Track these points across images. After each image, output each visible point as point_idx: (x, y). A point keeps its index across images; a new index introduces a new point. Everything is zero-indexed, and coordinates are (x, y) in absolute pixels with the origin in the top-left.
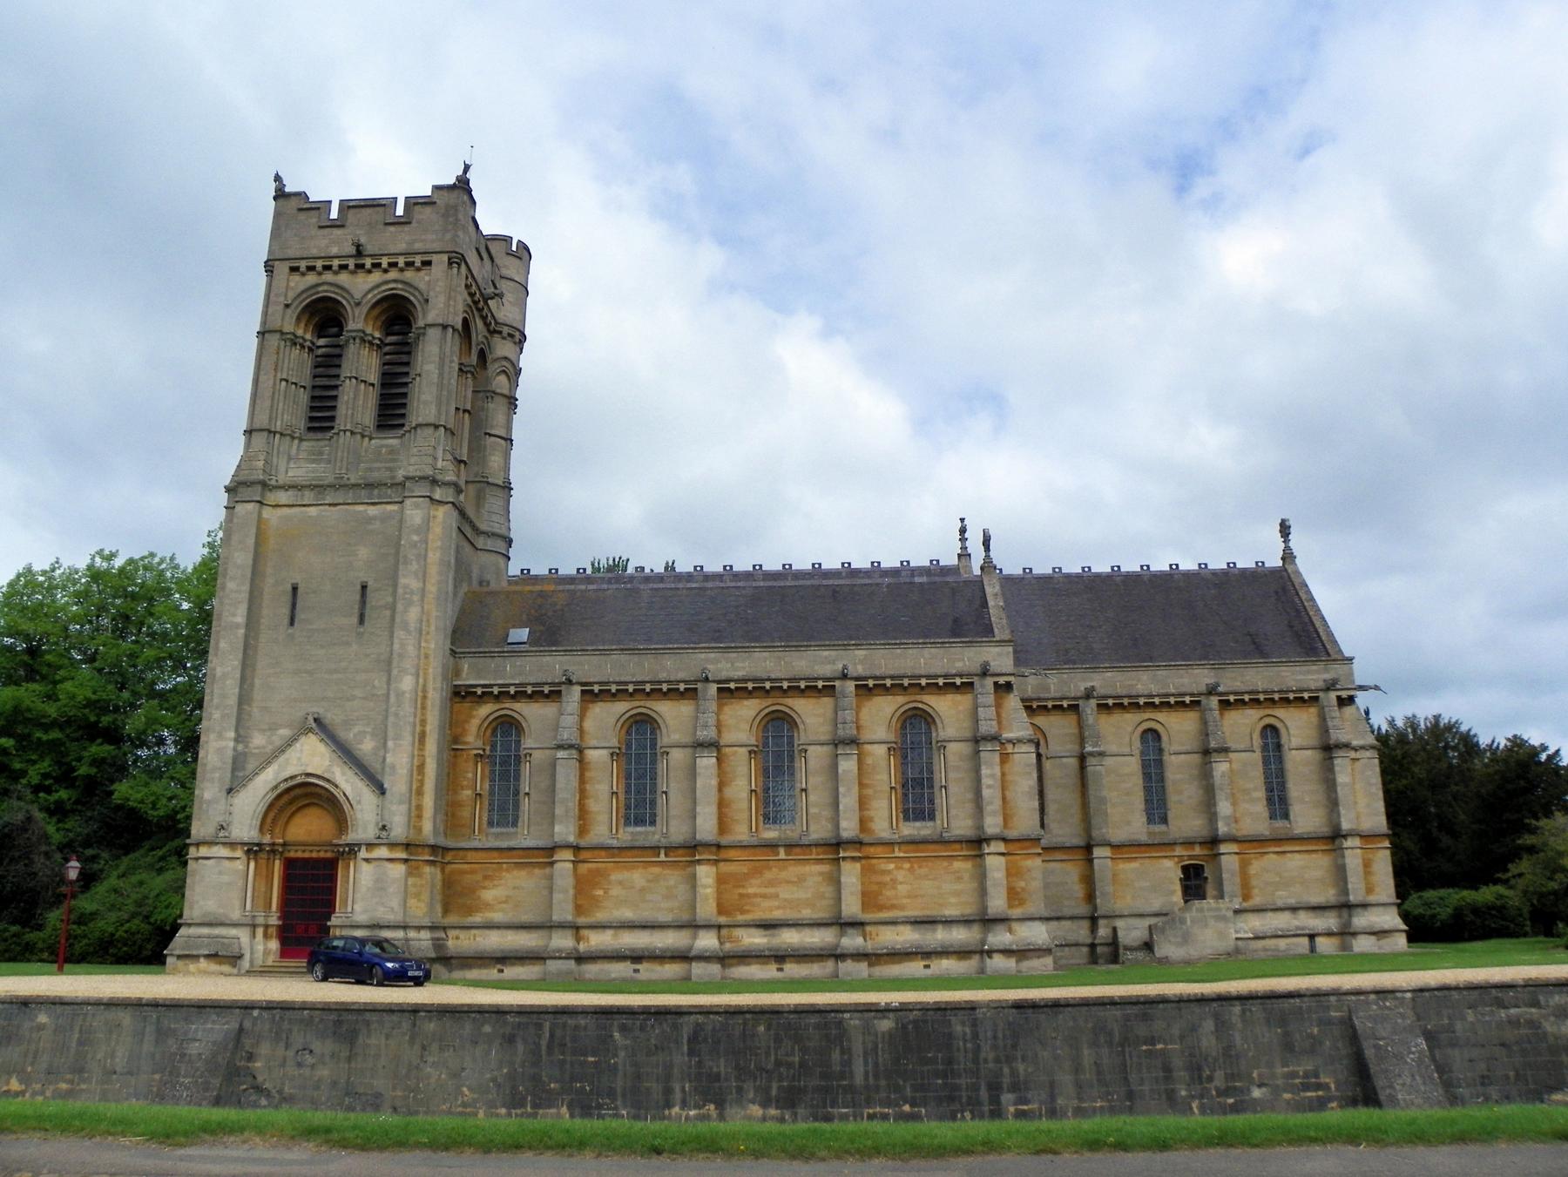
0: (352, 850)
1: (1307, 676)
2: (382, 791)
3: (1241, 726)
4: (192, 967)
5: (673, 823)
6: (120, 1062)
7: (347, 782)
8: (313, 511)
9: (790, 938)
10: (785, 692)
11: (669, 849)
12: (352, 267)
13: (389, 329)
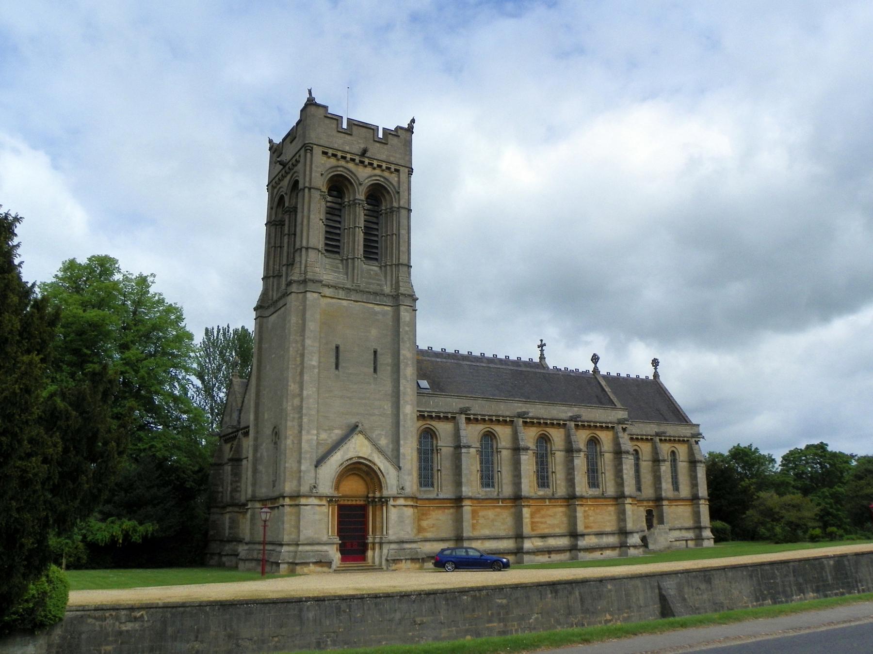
1: (672, 430)
3: (665, 449)
5: (504, 487)
6: (642, 603)
7: (381, 463)
8: (345, 303)
9: (552, 542)
11: (504, 500)
12: (357, 161)
13: (338, 197)
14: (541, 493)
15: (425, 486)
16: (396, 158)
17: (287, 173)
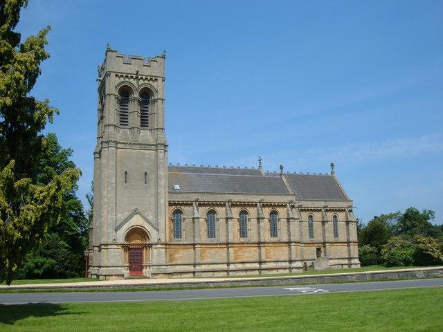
0: (150, 246)
2: (158, 230)
7: (148, 228)
10: (181, 205)
14: (274, 239)
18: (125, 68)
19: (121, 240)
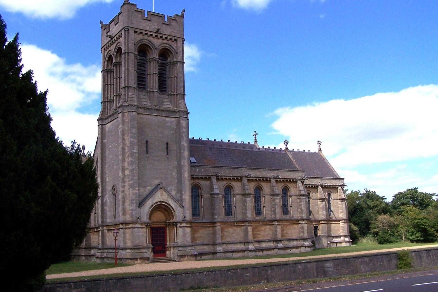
0: (175, 224)
4: (136, 262)
7: (173, 204)
9: (264, 245)
11: (238, 222)
12: (154, 36)
15: (195, 216)
16: (175, 33)
17: (113, 43)
18: (144, 25)
19: (145, 219)
